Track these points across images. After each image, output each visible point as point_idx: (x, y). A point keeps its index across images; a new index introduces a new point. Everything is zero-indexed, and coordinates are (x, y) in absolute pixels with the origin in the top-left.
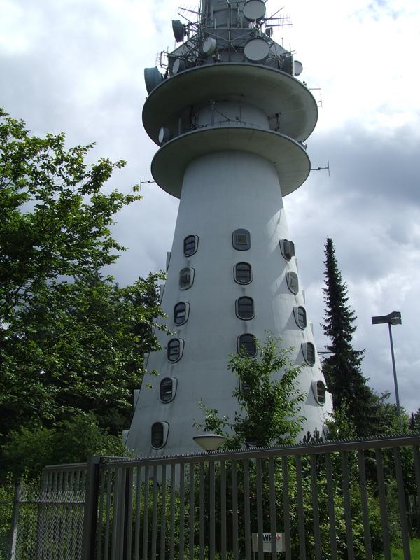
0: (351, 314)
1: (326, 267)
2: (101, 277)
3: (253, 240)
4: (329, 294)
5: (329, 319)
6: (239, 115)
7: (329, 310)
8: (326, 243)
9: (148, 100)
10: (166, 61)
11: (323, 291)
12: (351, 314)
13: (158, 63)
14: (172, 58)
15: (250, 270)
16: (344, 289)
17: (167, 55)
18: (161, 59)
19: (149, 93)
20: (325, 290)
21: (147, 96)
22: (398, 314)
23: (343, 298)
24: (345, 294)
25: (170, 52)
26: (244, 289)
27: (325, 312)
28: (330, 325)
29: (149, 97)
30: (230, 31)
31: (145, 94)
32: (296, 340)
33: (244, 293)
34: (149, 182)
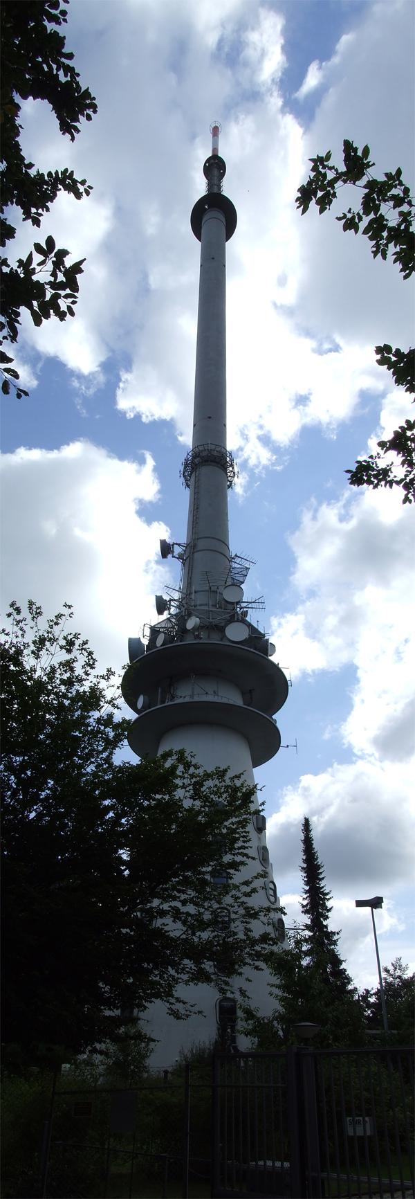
7: (307, 888)
10: (148, 632)
12: (328, 894)
20: (302, 868)
23: (321, 877)
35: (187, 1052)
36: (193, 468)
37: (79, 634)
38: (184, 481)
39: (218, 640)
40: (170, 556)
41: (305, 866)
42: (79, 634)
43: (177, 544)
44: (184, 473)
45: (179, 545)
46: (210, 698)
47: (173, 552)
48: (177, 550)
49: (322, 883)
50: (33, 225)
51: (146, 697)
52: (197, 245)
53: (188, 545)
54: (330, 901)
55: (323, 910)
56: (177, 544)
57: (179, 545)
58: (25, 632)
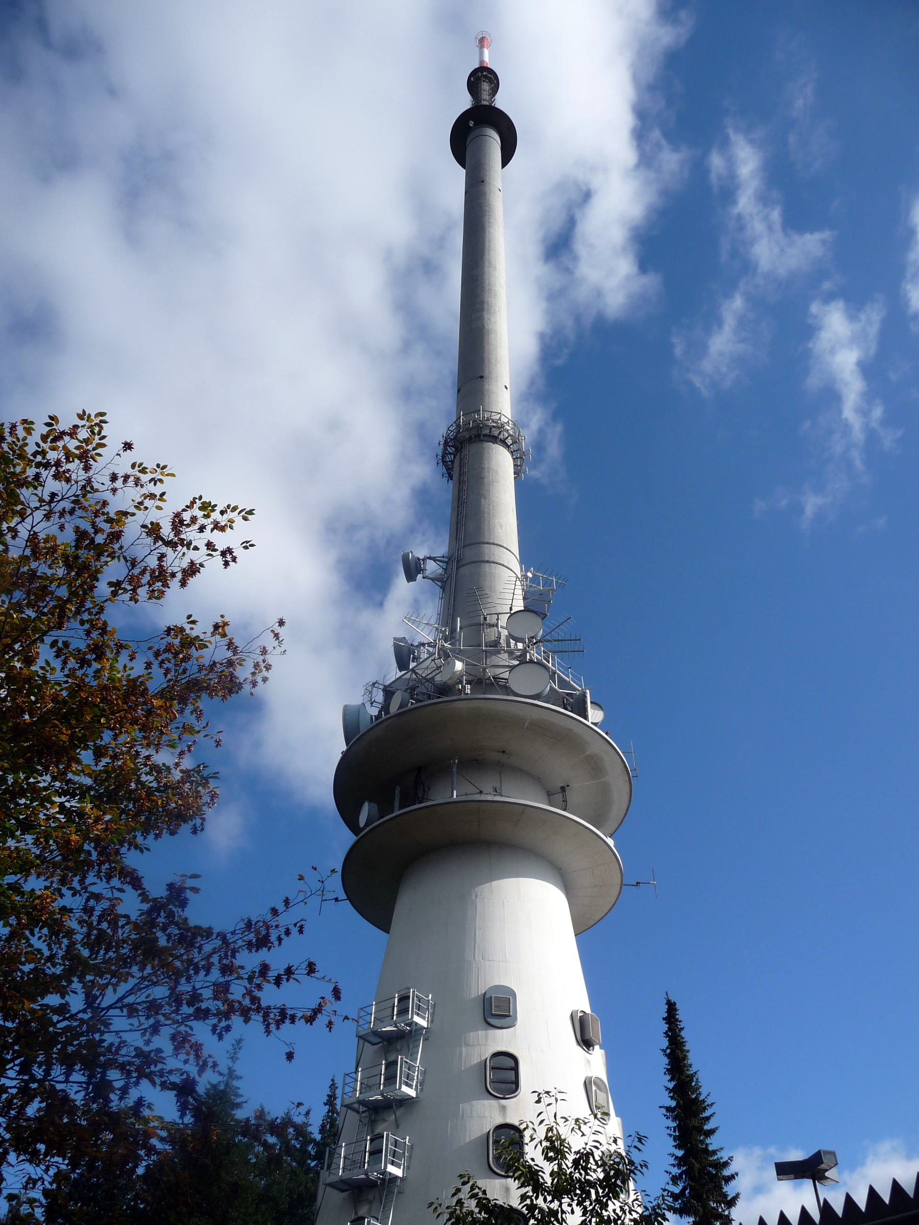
0: (714, 1152)
1: (666, 1061)
2: (145, 1101)
3: (522, 1008)
4: (674, 1119)
5: (681, 1174)
6: (497, 785)
7: (680, 1153)
8: (663, 1011)
9: (345, 755)
10: (379, 697)
11: (664, 1111)
12: (726, 1164)
13: (367, 698)
14: (389, 692)
15: (516, 1069)
16: (705, 1109)
17: (382, 687)
18: (371, 692)
19: (347, 743)
20: (668, 1109)
21: (344, 748)
22: (199, 889)
23: (706, 1127)
24: (708, 1119)
25: (387, 684)
26: (503, 1108)
27: (672, 1161)
28: (684, 1189)
29: (348, 751)
30: (486, 651)
31: (341, 746)
32: (488, 788)
33: (505, 1117)
34: (336, 900)
35: (487, 208)
36: (456, 449)
37: (267, 1036)
38: (445, 470)
39: (490, 1065)
40: (420, 576)
41: (673, 1104)
42: (267, 1036)
43: (430, 558)
44: (443, 457)
45: (434, 559)
46: (507, 344)
47: (424, 570)
48: (432, 567)
49: (713, 1143)
50: (189, 1007)
51: (374, 805)
52: (461, 173)
53: (450, 559)
54: (733, 1183)
55: (719, 1202)
56: (430, 558)
57: (434, 559)
58: (195, 499)
